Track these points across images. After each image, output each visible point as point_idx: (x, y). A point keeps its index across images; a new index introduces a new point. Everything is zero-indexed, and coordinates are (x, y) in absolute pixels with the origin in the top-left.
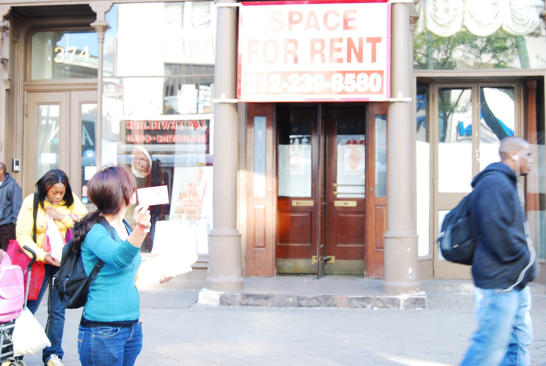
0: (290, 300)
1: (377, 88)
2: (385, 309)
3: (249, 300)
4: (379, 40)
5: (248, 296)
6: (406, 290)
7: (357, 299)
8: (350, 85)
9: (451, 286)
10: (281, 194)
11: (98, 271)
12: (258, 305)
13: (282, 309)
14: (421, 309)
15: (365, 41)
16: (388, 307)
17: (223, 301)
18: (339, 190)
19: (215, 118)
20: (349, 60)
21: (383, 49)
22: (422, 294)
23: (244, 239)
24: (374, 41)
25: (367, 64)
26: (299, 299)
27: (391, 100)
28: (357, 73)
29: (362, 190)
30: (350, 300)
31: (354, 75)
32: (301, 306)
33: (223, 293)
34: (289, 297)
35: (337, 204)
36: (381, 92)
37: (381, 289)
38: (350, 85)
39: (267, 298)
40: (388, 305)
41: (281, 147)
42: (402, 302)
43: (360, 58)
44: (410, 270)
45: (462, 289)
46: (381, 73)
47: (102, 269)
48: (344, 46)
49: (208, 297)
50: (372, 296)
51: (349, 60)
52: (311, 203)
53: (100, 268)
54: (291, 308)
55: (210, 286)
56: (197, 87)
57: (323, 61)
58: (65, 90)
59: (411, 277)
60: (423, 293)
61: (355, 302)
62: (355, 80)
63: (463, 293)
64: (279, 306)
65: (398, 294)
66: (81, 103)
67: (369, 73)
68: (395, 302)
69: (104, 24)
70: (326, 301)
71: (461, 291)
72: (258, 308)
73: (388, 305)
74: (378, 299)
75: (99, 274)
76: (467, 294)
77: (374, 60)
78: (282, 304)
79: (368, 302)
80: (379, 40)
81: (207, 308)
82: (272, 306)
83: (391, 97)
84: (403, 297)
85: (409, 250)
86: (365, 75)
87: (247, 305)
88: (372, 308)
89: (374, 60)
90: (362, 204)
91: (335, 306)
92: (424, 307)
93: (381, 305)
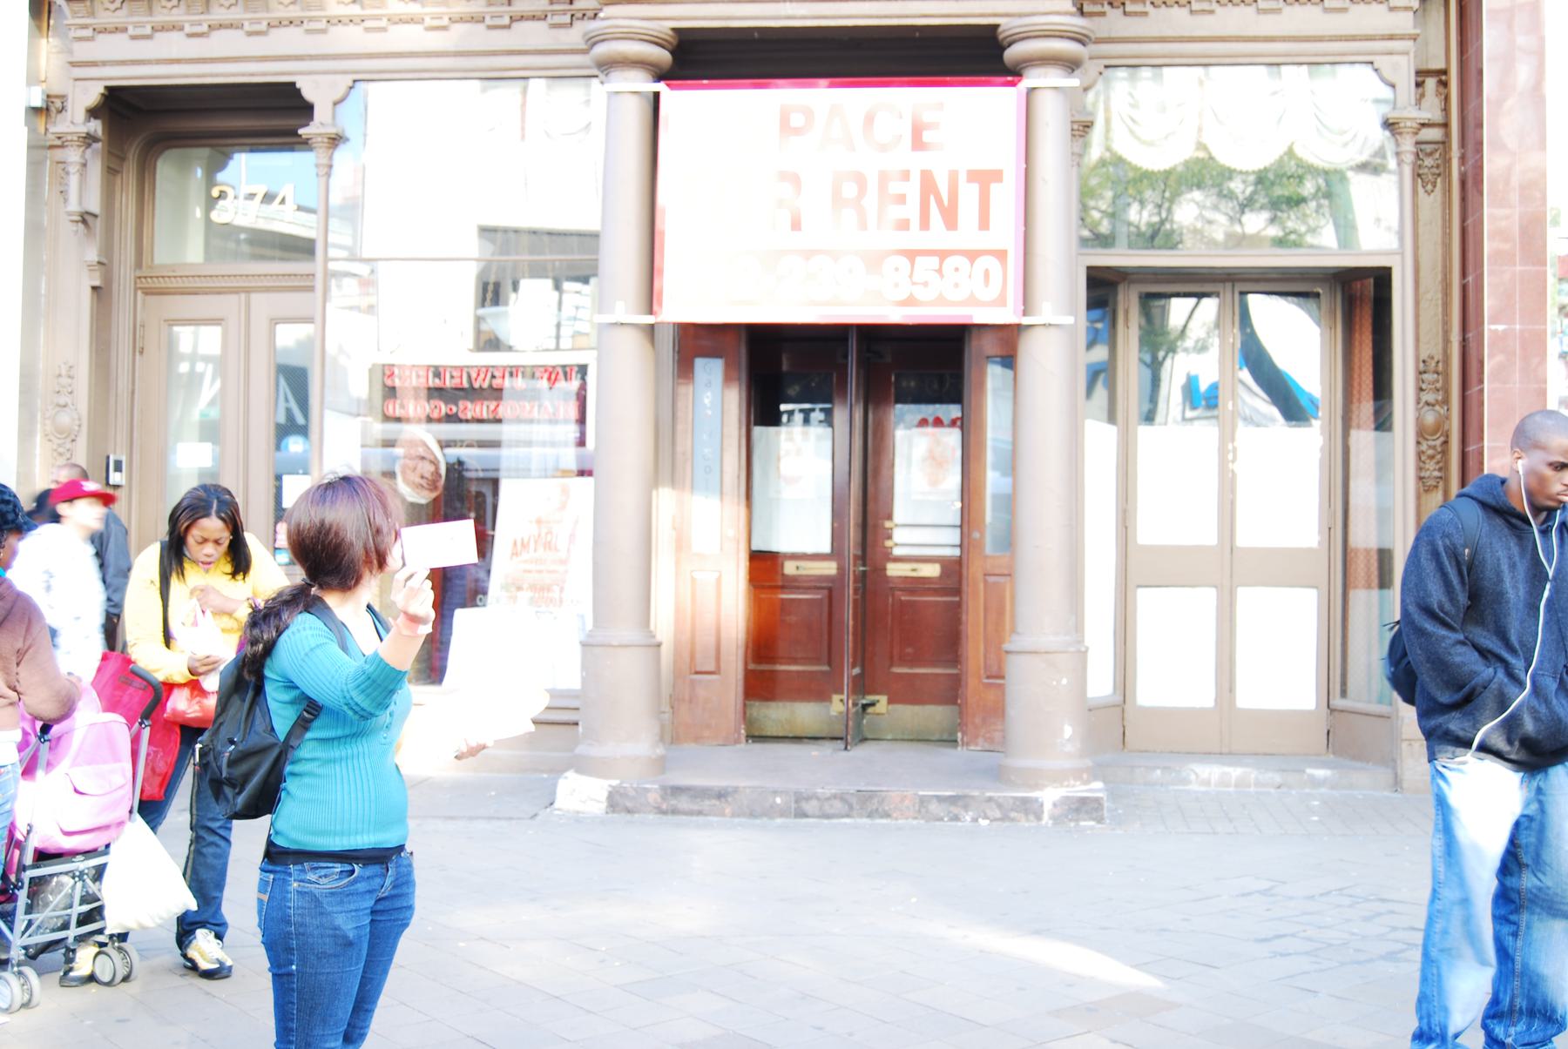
0: (778, 800)
1: (993, 292)
2: (1007, 824)
3: (679, 801)
4: (997, 176)
5: (677, 791)
6: (1058, 778)
7: (940, 799)
8: (926, 284)
9: (1165, 768)
10: (758, 545)
11: (306, 729)
12: (700, 813)
13: (758, 821)
14: (1092, 823)
15: (962, 178)
16: (1013, 820)
17: (615, 802)
18: (899, 536)
19: (599, 360)
20: (925, 224)
21: (1006, 198)
22: (1096, 789)
23: (666, 652)
24: (985, 179)
25: (968, 234)
26: (799, 798)
27: (1025, 321)
28: (943, 255)
29: (954, 537)
30: (923, 801)
31: (935, 260)
32: (805, 815)
33: (615, 782)
34: (775, 793)
35: (893, 570)
36: (1001, 301)
37: (999, 775)
38: (926, 284)
39: (721, 795)
40: (1013, 814)
41: (758, 431)
42: (1048, 807)
43: (951, 221)
44: (1068, 731)
45: (1193, 777)
46: (1001, 255)
47: (316, 724)
48: (913, 190)
49: (581, 793)
50: (976, 793)
51: (925, 224)
52: (830, 568)
53: (311, 721)
54: (779, 821)
55: (584, 766)
56: (558, 287)
57: (863, 225)
58: (235, 291)
59: (1069, 748)
60: (1098, 785)
61: (934, 807)
62: (940, 271)
63: (1194, 787)
64: (752, 815)
65: (1036, 787)
66: (275, 322)
67: (972, 255)
68: (1030, 808)
69: (332, 130)
70: (866, 804)
71: (1189, 782)
72: (701, 819)
73: (1013, 814)
74: (990, 799)
75: (309, 735)
76: (1203, 789)
77: (984, 224)
78: (758, 811)
79: (966, 808)
80: (997, 176)
81: (578, 819)
82: (733, 815)
83: (1025, 313)
84: (1049, 796)
85: (1064, 681)
86: (961, 261)
87: (675, 812)
88: (975, 820)
89: (984, 224)
90: (954, 570)
91: (887, 815)
92: (1100, 820)
93: (998, 814)
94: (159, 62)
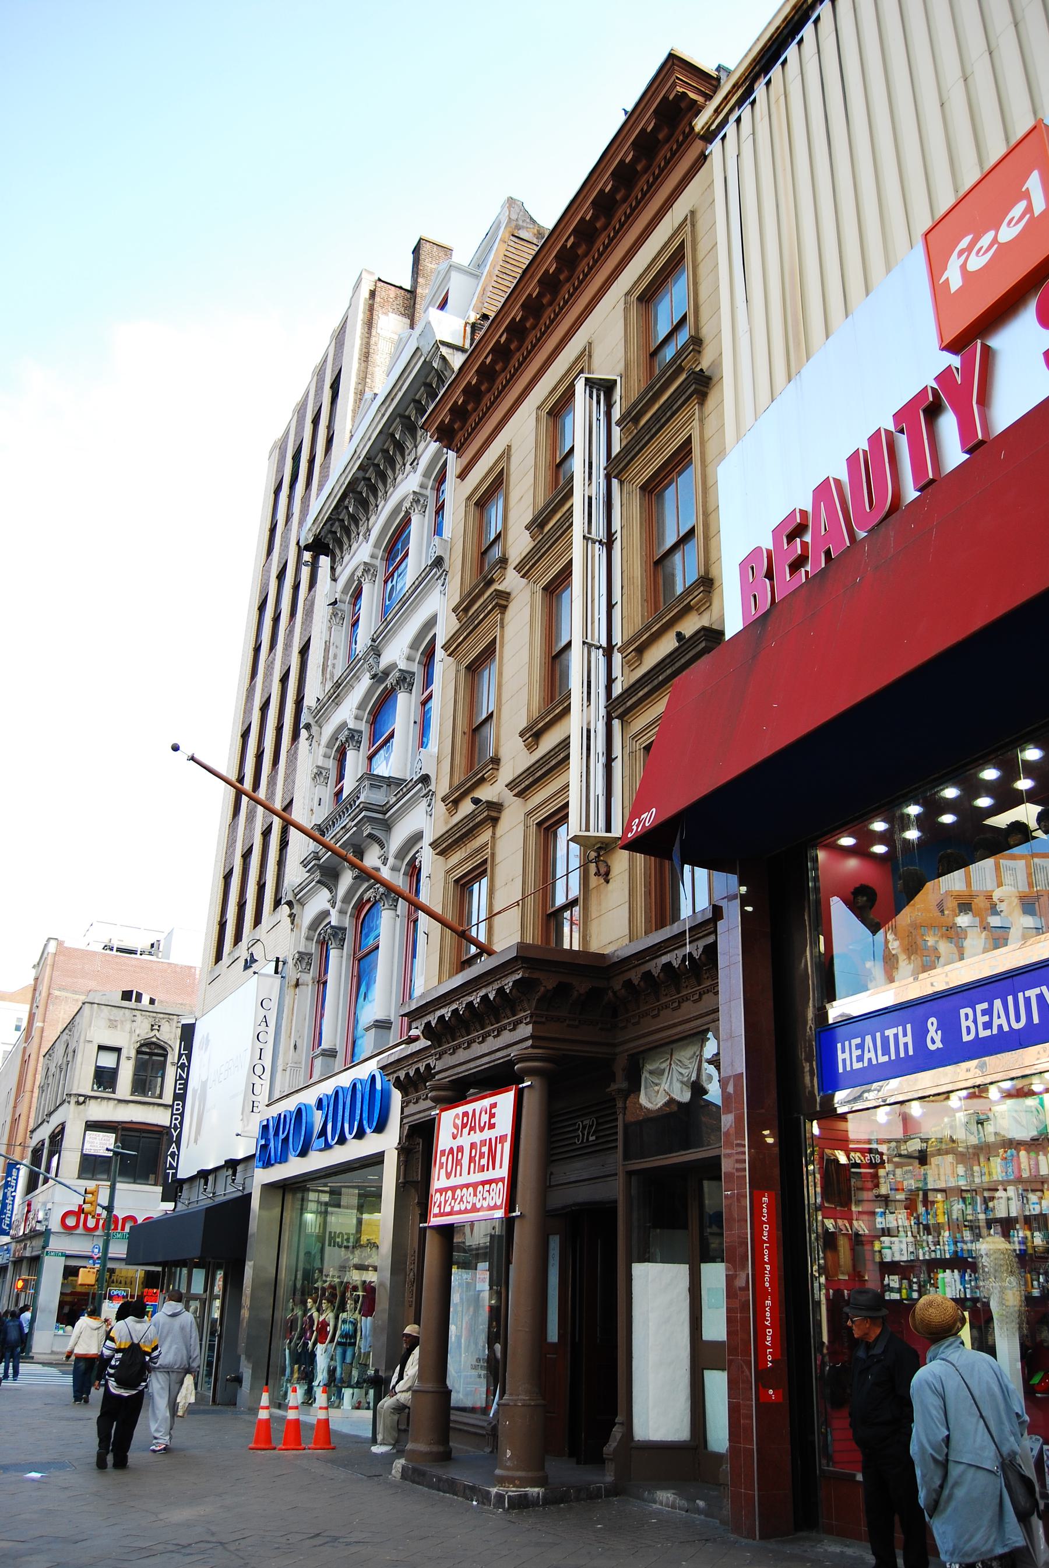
44: (509, 1453)
59: (508, 1464)
94: (420, 1112)
